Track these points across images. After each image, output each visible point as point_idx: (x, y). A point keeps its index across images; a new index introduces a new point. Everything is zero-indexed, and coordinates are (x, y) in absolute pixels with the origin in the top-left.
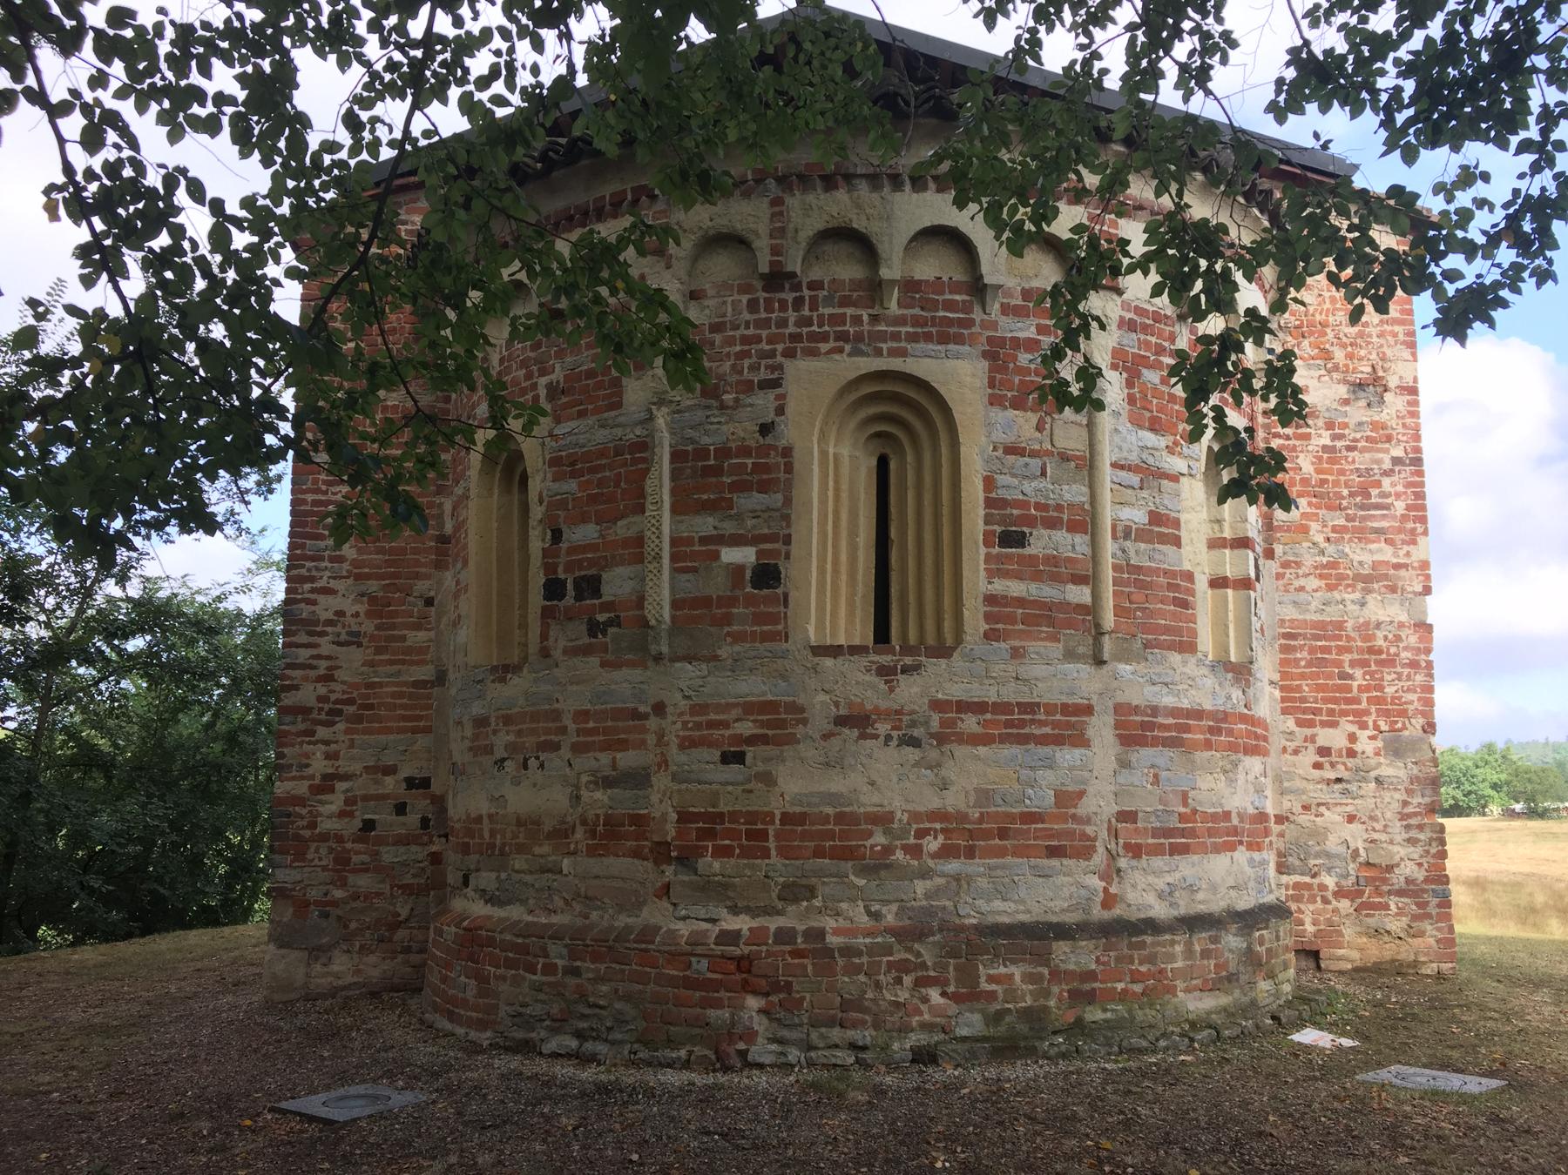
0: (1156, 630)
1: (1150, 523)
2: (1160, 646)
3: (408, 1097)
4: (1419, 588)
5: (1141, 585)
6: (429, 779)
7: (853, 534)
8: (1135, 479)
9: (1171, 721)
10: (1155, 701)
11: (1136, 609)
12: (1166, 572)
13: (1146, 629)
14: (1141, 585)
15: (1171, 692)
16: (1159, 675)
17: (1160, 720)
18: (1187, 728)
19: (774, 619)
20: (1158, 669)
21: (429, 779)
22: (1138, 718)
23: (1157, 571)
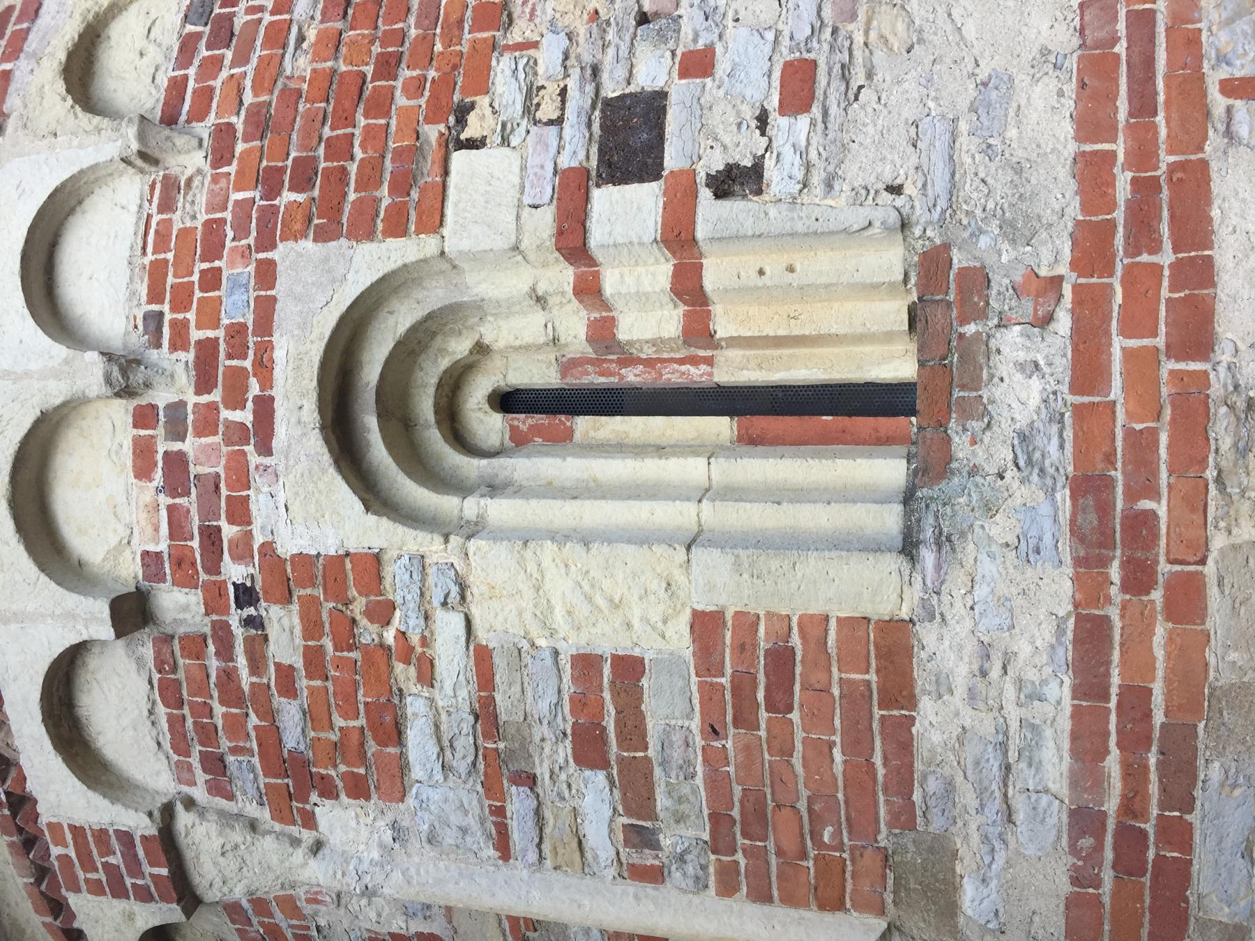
0: (860, 775)
1: (604, 764)
2: (903, 779)
3: (955, 310)
4: (492, 254)
5: (756, 821)
6: (709, 51)
7: (661, 450)
8: (518, 802)
9: (1113, 763)
10: (1057, 816)
11: (818, 843)
12: (714, 731)
13: (863, 824)
14: (756, 821)
15: (1029, 753)
16: (982, 792)
17: (1111, 805)
18: (1137, 699)
19: (781, 659)
20: (967, 797)
21: (709, 51)
22: (1108, 876)
23: (713, 759)
